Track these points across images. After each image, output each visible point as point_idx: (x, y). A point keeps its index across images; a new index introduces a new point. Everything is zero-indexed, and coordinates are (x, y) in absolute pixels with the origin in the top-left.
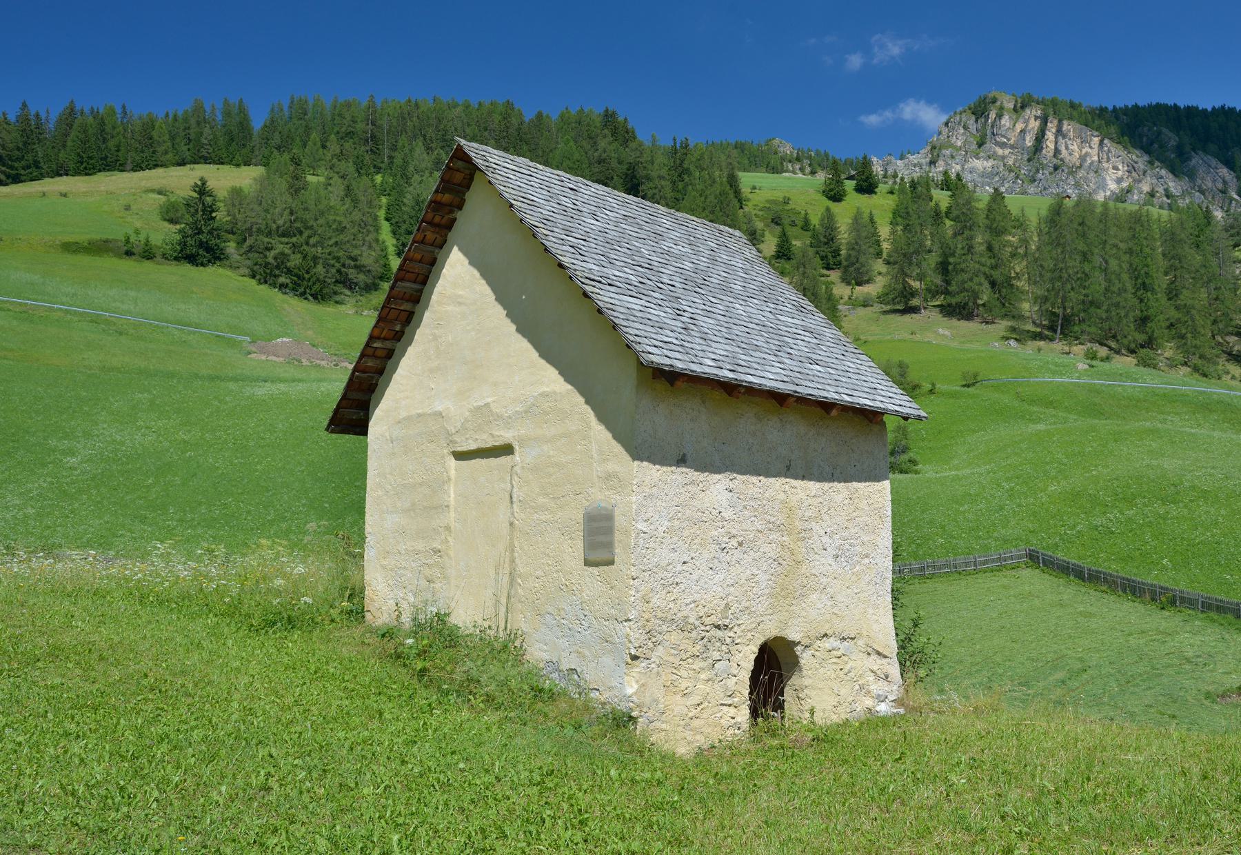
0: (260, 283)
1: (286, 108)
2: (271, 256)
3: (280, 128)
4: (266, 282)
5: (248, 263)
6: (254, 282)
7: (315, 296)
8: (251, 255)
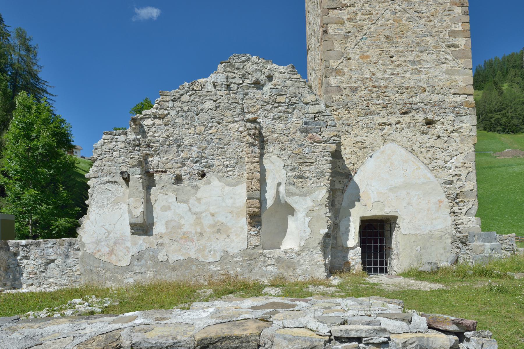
0: (488, 131)
1: (483, 66)
2: (493, 120)
3: (482, 74)
4: (491, 131)
5: (482, 125)
6: (486, 132)
7: (513, 132)
8: (483, 122)
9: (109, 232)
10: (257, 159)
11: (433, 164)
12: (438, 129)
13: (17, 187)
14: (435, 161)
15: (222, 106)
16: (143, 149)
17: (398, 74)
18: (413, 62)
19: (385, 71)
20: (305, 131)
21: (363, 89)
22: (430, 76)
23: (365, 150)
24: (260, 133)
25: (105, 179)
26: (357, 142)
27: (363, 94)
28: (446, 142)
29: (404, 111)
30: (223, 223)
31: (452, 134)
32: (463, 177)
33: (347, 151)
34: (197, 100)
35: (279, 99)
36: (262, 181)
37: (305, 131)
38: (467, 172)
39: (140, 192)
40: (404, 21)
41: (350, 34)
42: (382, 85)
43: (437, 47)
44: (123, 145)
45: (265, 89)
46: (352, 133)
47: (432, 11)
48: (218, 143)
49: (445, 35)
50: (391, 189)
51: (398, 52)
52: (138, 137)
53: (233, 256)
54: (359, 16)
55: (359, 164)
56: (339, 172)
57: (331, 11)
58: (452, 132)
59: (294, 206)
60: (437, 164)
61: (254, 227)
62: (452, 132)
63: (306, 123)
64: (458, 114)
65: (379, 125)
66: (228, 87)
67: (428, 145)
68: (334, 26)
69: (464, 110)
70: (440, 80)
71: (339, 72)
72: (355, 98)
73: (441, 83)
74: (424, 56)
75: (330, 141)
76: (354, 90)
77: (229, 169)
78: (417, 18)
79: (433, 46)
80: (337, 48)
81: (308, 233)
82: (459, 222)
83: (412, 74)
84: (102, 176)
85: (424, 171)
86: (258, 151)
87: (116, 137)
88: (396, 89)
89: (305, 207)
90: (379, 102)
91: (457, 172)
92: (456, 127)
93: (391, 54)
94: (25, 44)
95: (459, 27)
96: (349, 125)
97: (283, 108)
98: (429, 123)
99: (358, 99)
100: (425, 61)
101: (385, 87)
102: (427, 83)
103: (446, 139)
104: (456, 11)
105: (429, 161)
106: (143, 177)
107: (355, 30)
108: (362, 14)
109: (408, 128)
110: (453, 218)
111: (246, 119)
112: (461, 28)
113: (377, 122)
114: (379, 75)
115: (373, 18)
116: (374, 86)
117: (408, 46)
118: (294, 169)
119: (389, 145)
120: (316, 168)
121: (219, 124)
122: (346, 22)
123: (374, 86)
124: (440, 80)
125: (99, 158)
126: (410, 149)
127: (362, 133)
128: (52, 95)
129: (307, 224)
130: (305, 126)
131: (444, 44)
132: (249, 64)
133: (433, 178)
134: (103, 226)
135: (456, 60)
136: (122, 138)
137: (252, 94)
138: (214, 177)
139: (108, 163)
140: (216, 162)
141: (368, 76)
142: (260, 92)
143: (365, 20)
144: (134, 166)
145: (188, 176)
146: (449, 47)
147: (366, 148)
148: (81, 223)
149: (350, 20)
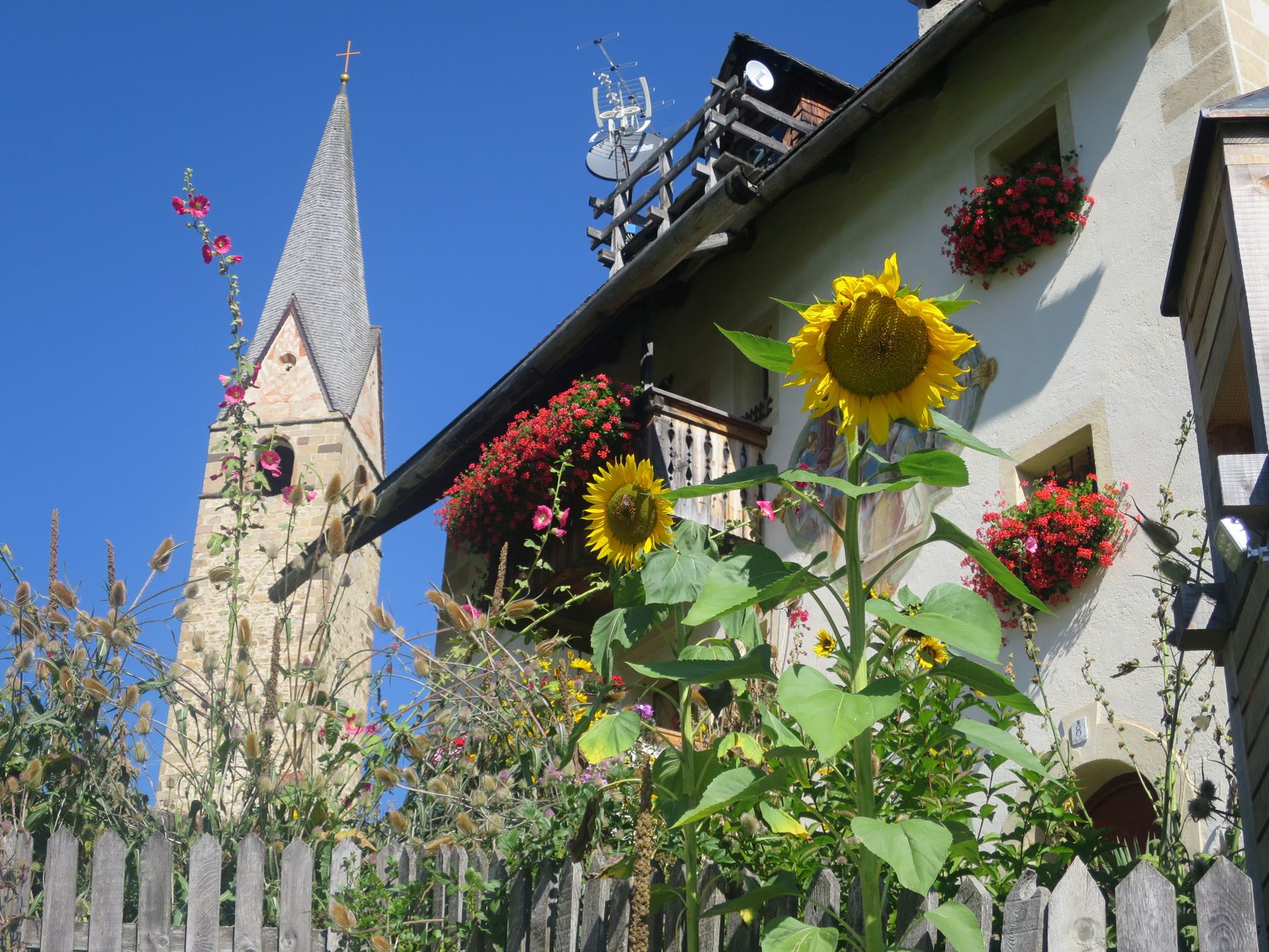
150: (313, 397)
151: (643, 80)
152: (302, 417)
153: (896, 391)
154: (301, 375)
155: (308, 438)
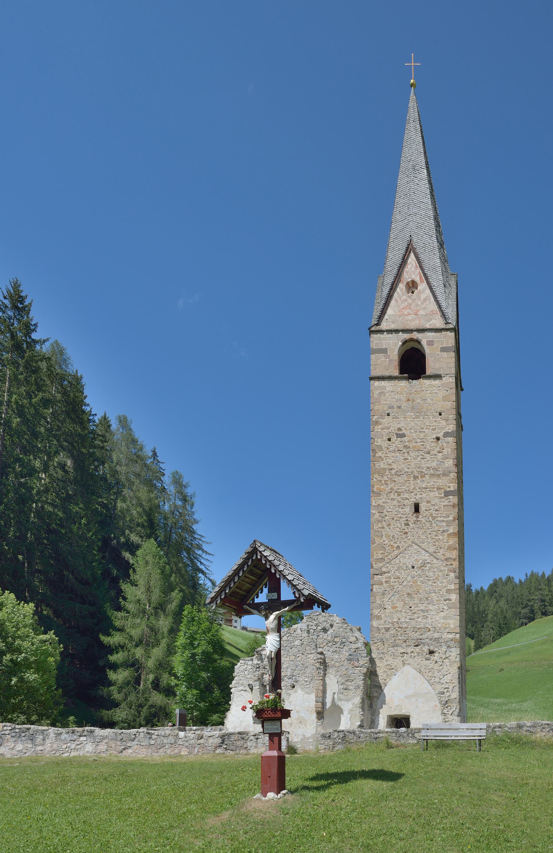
9: (241, 722)
10: (321, 678)
11: (432, 681)
12: (436, 656)
13: (183, 688)
14: (434, 678)
15: (305, 643)
16: (261, 670)
17: (414, 619)
18: (423, 611)
19: (406, 617)
20: (349, 660)
21: (392, 629)
22: (433, 620)
23: (392, 670)
24: (325, 661)
25: (240, 688)
26: (388, 665)
27: (392, 632)
28: (441, 665)
29: (416, 644)
30: (303, 717)
31: (445, 660)
32: (450, 690)
33: (381, 671)
34: (291, 639)
35: (336, 640)
36: (324, 692)
37: (349, 660)
38: (453, 686)
39: (258, 697)
40: (419, 583)
41: (386, 592)
42: (404, 626)
43: (438, 601)
44: (250, 667)
45: (329, 633)
46: (385, 659)
47: (436, 576)
48: (302, 667)
49: (443, 592)
50: (407, 697)
51: (415, 604)
52: (259, 662)
53: (308, 739)
54: (392, 580)
55: (388, 680)
56: (376, 685)
57: (375, 576)
58: (445, 659)
59: (342, 707)
60: (435, 681)
61: (320, 720)
62: (445, 659)
63: (350, 655)
64: (449, 647)
65: (401, 653)
66: (308, 632)
67: (430, 668)
68: (377, 586)
69: (452, 644)
70: (439, 623)
71: (379, 618)
72: (387, 635)
73: (440, 625)
74: (430, 607)
75: (364, 667)
76: (387, 630)
77: (307, 683)
78: (426, 581)
79: (436, 600)
80: (378, 602)
81: (349, 725)
82: (447, 720)
83: (422, 619)
84: (239, 686)
85: (426, 685)
86: (322, 673)
87: (247, 662)
88: (412, 629)
89: (348, 708)
90: (402, 638)
91: (447, 686)
92: (447, 656)
93: (410, 605)
94: (182, 493)
95: (452, 587)
96: (383, 653)
97: (338, 645)
98: (431, 652)
99: (389, 636)
100: (430, 610)
101: (406, 628)
102: (432, 625)
103: (441, 664)
104: (451, 576)
105: (430, 678)
106: (261, 688)
107: (390, 589)
108: (394, 578)
109: (418, 656)
110: (443, 717)
111: (317, 651)
112: (453, 588)
113: (400, 652)
114: (402, 620)
115: (400, 581)
116: (399, 627)
117: (421, 599)
118: (343, 684)
119: (407, 667)
120: (355, 684)
121: (303, 654)
122: (384, 584)
123: (399, 627)
124: (439, 623)
125: (238, 675)
126: (419, 670)
127: (391, 659)
128: (209, 554)
129: (349, 718)
130: (350, 657)
131: (443, 599)
132: (320, 617)
133: (432, 690)
134: (238, 718)
135: (450, 610)
136: (250, 663)
137: (322, 636)
138: (299, 688)
139: (242, 678)
140: (300, 679)
141: (396, 621)
142: (326, 634)
143: (395, 582)
144: (256, 681)
145: (285, 687)
146: (445, 600)
147: (393, 669)
148: (227, 716)
149: (386, 582)
150: (432, 313)
151: (420, 64)
152: (428, 326)
153: (165, 709)
154: (423, 296)
155: (433, 341)
